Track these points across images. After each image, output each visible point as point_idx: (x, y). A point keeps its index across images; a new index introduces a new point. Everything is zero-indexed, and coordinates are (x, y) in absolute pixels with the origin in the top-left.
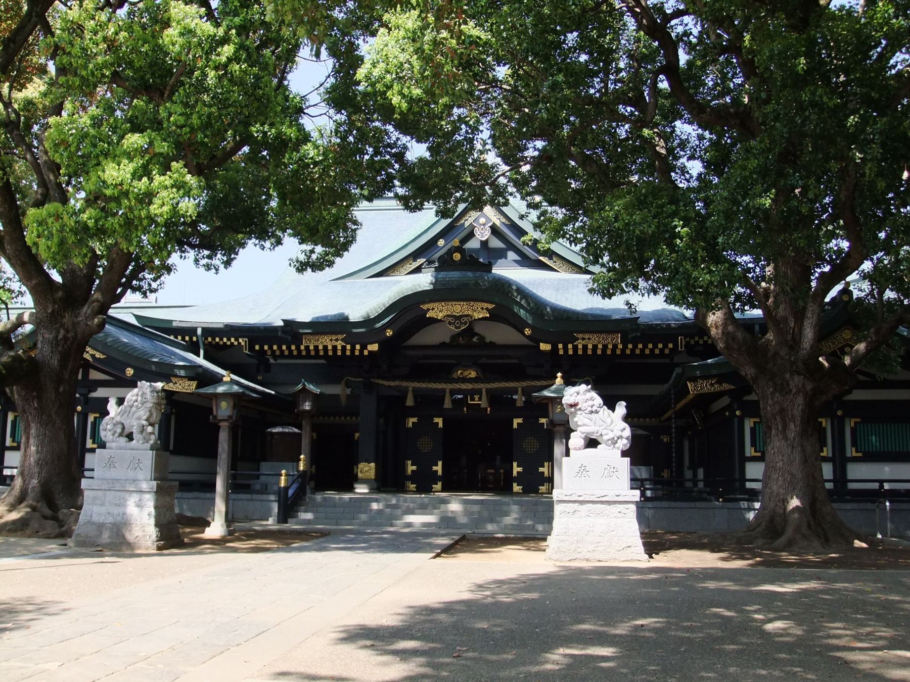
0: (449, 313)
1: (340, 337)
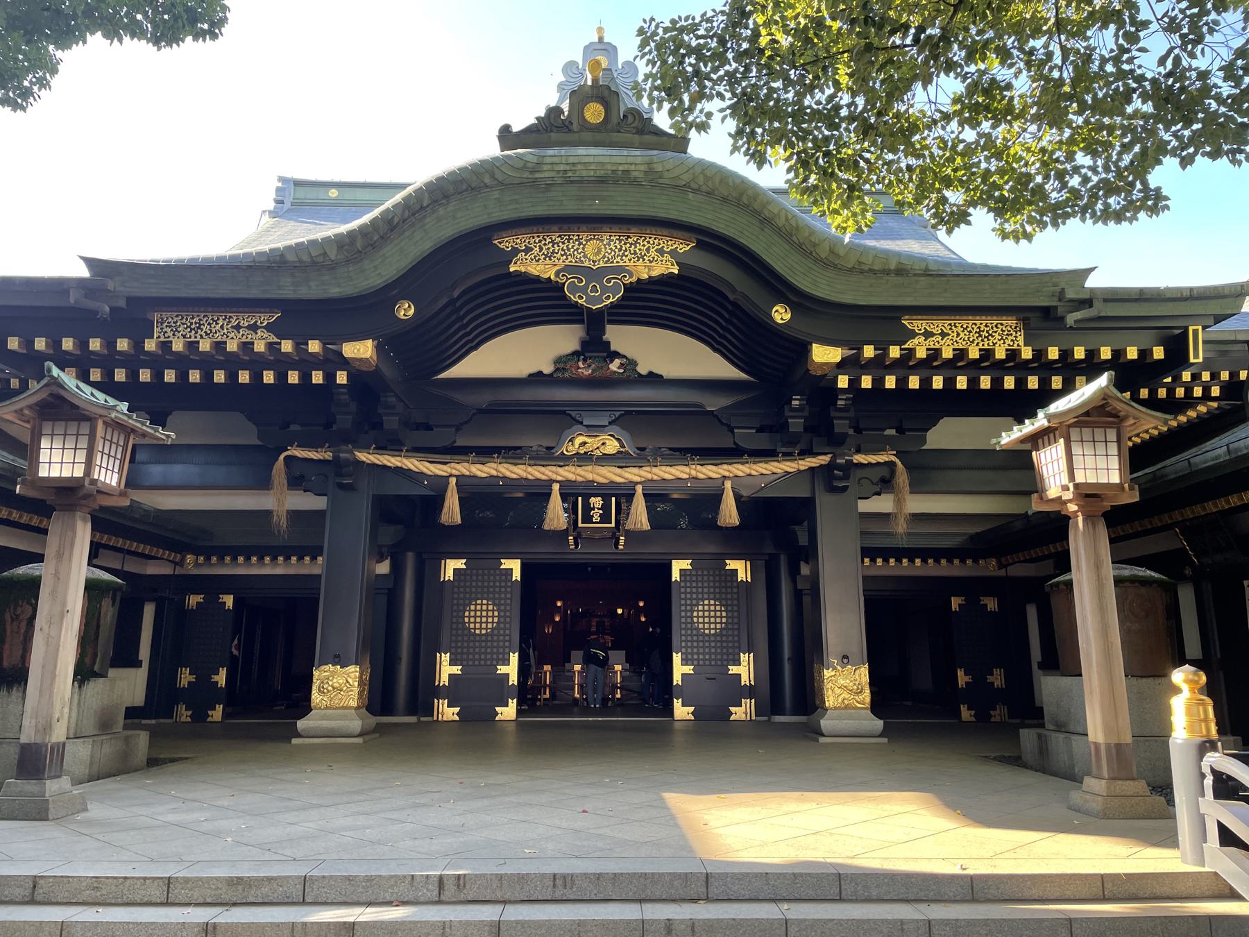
0: (571, 261)
1: (265, 319)
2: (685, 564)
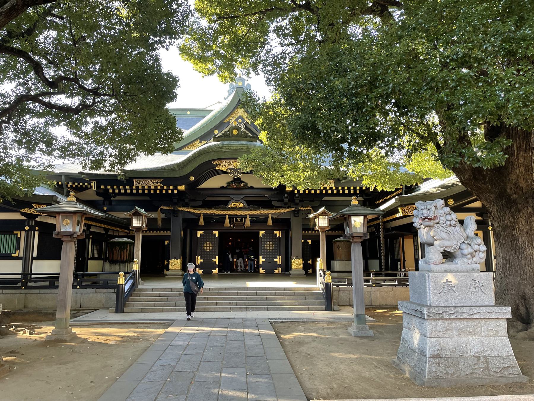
0: (230, 167)
1: (159, 181)
2: (263, 232)
